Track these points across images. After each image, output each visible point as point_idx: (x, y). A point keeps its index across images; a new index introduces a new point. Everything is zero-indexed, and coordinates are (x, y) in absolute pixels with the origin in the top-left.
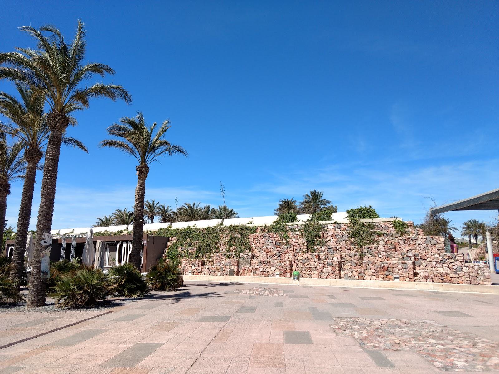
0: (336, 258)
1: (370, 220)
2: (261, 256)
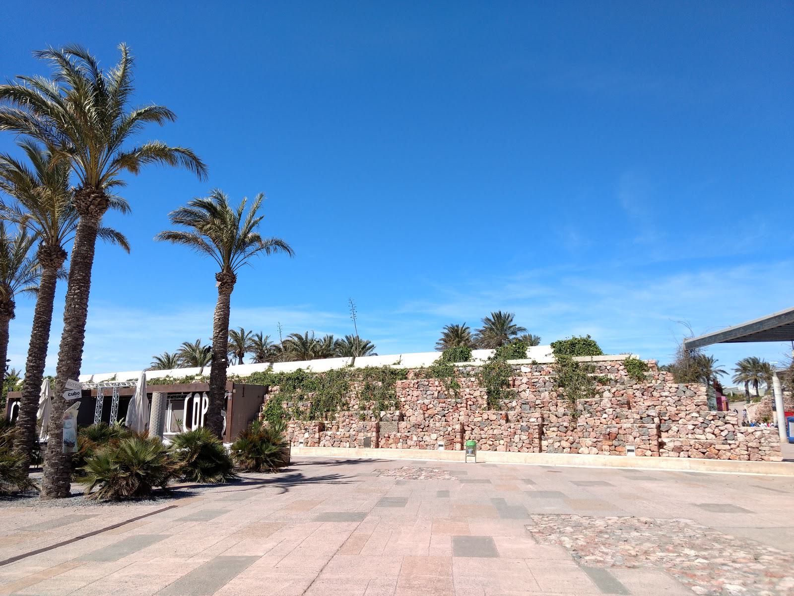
0: (534, 418)
1: (588, 358)
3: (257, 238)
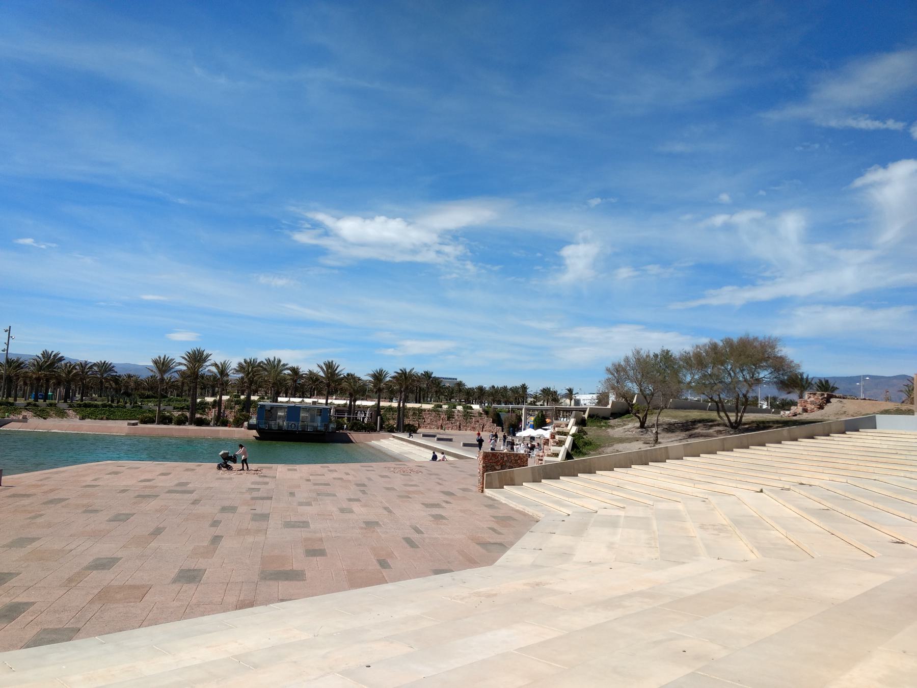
0: (458, 424)
1: (470, 411)
2: (428, 421)
3: (113, 370)
